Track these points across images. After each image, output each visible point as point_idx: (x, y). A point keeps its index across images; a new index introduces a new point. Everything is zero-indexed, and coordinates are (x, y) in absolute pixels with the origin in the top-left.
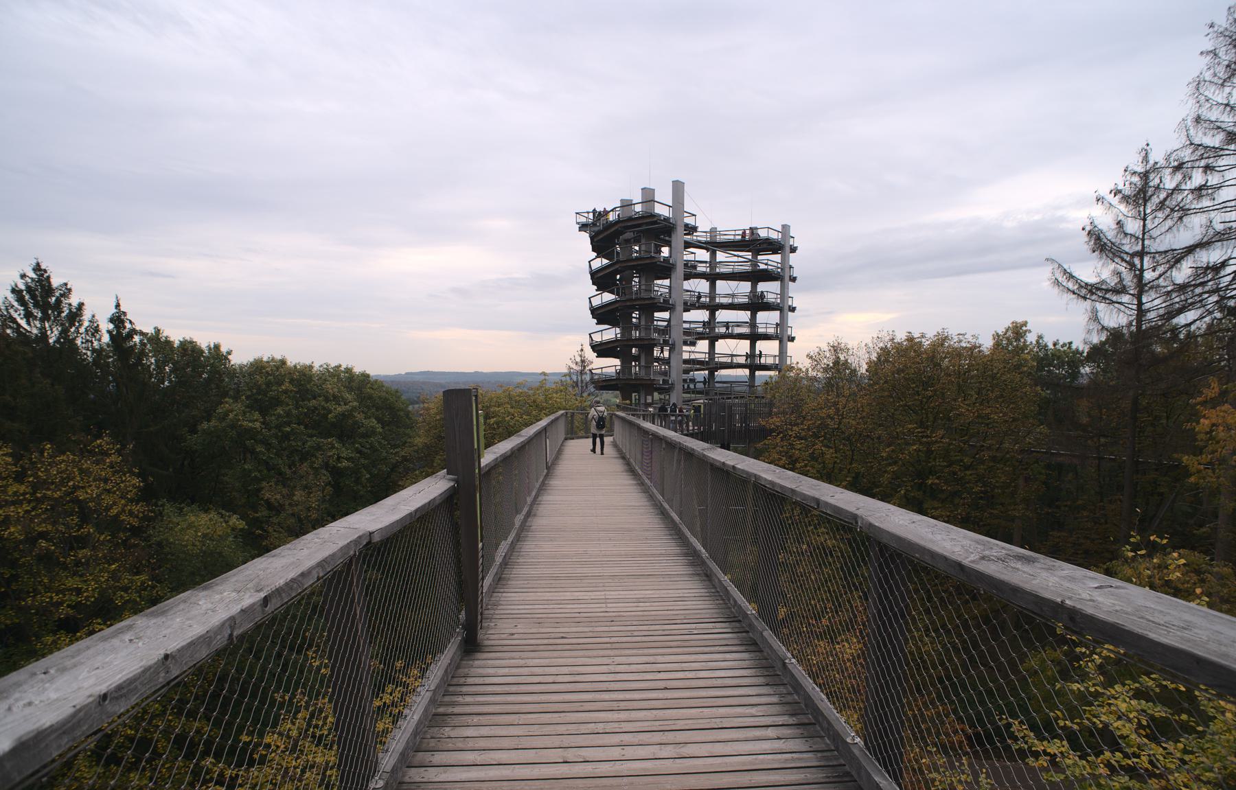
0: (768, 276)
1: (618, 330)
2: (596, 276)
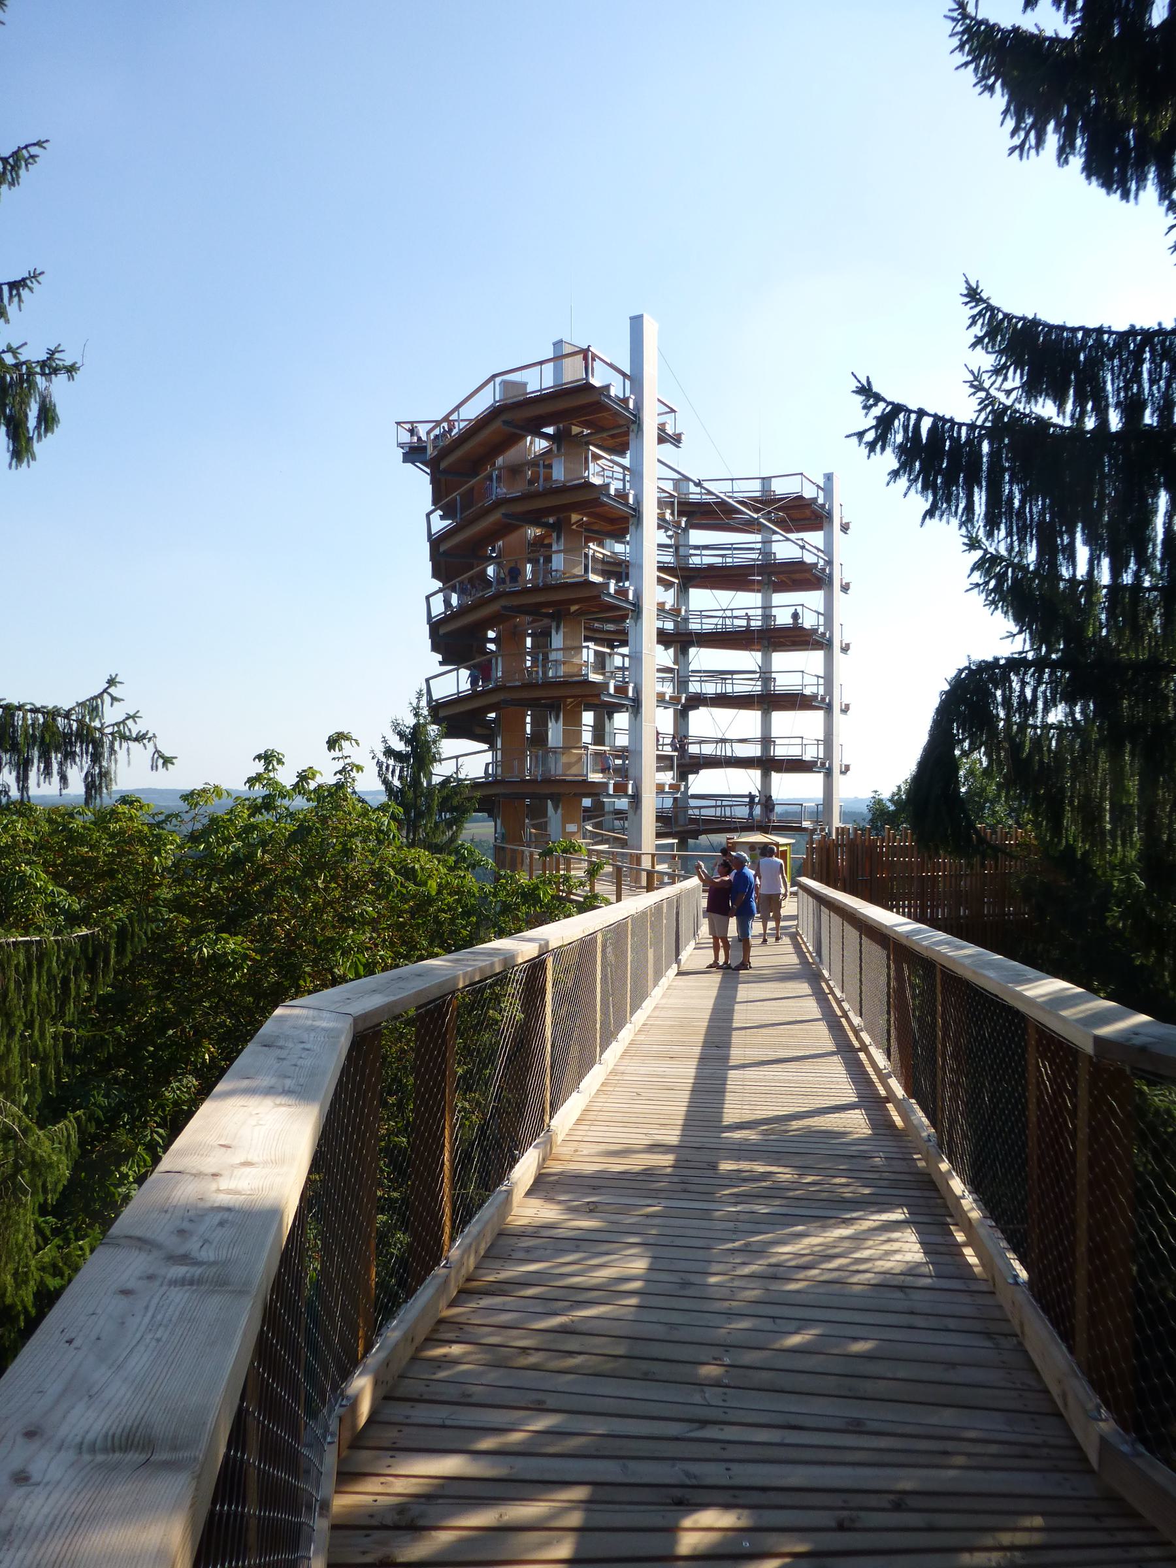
0: (796, 701)
1: (464, 673)
2: (442, 631)
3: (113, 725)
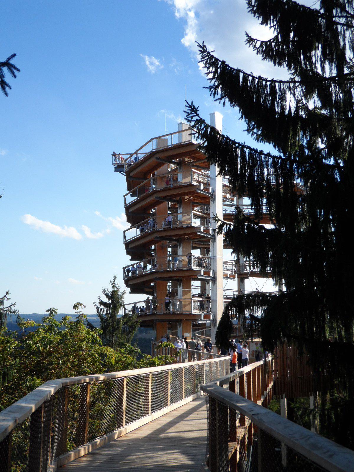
2: (130, 246)
3: (7, 308)
